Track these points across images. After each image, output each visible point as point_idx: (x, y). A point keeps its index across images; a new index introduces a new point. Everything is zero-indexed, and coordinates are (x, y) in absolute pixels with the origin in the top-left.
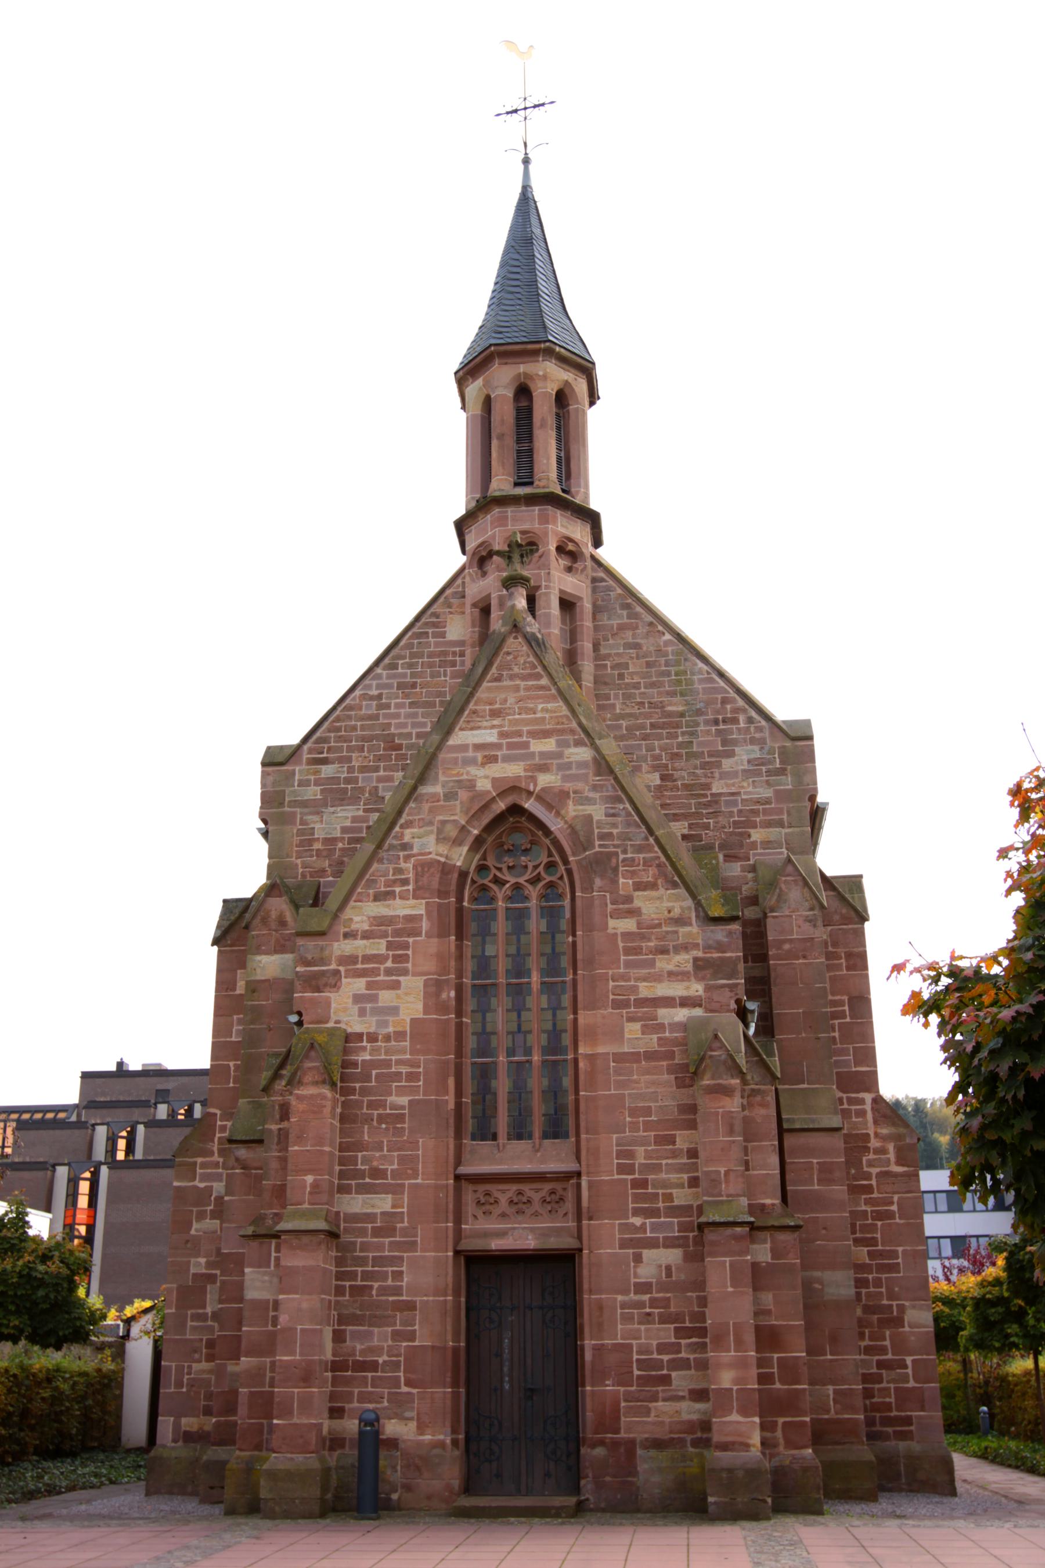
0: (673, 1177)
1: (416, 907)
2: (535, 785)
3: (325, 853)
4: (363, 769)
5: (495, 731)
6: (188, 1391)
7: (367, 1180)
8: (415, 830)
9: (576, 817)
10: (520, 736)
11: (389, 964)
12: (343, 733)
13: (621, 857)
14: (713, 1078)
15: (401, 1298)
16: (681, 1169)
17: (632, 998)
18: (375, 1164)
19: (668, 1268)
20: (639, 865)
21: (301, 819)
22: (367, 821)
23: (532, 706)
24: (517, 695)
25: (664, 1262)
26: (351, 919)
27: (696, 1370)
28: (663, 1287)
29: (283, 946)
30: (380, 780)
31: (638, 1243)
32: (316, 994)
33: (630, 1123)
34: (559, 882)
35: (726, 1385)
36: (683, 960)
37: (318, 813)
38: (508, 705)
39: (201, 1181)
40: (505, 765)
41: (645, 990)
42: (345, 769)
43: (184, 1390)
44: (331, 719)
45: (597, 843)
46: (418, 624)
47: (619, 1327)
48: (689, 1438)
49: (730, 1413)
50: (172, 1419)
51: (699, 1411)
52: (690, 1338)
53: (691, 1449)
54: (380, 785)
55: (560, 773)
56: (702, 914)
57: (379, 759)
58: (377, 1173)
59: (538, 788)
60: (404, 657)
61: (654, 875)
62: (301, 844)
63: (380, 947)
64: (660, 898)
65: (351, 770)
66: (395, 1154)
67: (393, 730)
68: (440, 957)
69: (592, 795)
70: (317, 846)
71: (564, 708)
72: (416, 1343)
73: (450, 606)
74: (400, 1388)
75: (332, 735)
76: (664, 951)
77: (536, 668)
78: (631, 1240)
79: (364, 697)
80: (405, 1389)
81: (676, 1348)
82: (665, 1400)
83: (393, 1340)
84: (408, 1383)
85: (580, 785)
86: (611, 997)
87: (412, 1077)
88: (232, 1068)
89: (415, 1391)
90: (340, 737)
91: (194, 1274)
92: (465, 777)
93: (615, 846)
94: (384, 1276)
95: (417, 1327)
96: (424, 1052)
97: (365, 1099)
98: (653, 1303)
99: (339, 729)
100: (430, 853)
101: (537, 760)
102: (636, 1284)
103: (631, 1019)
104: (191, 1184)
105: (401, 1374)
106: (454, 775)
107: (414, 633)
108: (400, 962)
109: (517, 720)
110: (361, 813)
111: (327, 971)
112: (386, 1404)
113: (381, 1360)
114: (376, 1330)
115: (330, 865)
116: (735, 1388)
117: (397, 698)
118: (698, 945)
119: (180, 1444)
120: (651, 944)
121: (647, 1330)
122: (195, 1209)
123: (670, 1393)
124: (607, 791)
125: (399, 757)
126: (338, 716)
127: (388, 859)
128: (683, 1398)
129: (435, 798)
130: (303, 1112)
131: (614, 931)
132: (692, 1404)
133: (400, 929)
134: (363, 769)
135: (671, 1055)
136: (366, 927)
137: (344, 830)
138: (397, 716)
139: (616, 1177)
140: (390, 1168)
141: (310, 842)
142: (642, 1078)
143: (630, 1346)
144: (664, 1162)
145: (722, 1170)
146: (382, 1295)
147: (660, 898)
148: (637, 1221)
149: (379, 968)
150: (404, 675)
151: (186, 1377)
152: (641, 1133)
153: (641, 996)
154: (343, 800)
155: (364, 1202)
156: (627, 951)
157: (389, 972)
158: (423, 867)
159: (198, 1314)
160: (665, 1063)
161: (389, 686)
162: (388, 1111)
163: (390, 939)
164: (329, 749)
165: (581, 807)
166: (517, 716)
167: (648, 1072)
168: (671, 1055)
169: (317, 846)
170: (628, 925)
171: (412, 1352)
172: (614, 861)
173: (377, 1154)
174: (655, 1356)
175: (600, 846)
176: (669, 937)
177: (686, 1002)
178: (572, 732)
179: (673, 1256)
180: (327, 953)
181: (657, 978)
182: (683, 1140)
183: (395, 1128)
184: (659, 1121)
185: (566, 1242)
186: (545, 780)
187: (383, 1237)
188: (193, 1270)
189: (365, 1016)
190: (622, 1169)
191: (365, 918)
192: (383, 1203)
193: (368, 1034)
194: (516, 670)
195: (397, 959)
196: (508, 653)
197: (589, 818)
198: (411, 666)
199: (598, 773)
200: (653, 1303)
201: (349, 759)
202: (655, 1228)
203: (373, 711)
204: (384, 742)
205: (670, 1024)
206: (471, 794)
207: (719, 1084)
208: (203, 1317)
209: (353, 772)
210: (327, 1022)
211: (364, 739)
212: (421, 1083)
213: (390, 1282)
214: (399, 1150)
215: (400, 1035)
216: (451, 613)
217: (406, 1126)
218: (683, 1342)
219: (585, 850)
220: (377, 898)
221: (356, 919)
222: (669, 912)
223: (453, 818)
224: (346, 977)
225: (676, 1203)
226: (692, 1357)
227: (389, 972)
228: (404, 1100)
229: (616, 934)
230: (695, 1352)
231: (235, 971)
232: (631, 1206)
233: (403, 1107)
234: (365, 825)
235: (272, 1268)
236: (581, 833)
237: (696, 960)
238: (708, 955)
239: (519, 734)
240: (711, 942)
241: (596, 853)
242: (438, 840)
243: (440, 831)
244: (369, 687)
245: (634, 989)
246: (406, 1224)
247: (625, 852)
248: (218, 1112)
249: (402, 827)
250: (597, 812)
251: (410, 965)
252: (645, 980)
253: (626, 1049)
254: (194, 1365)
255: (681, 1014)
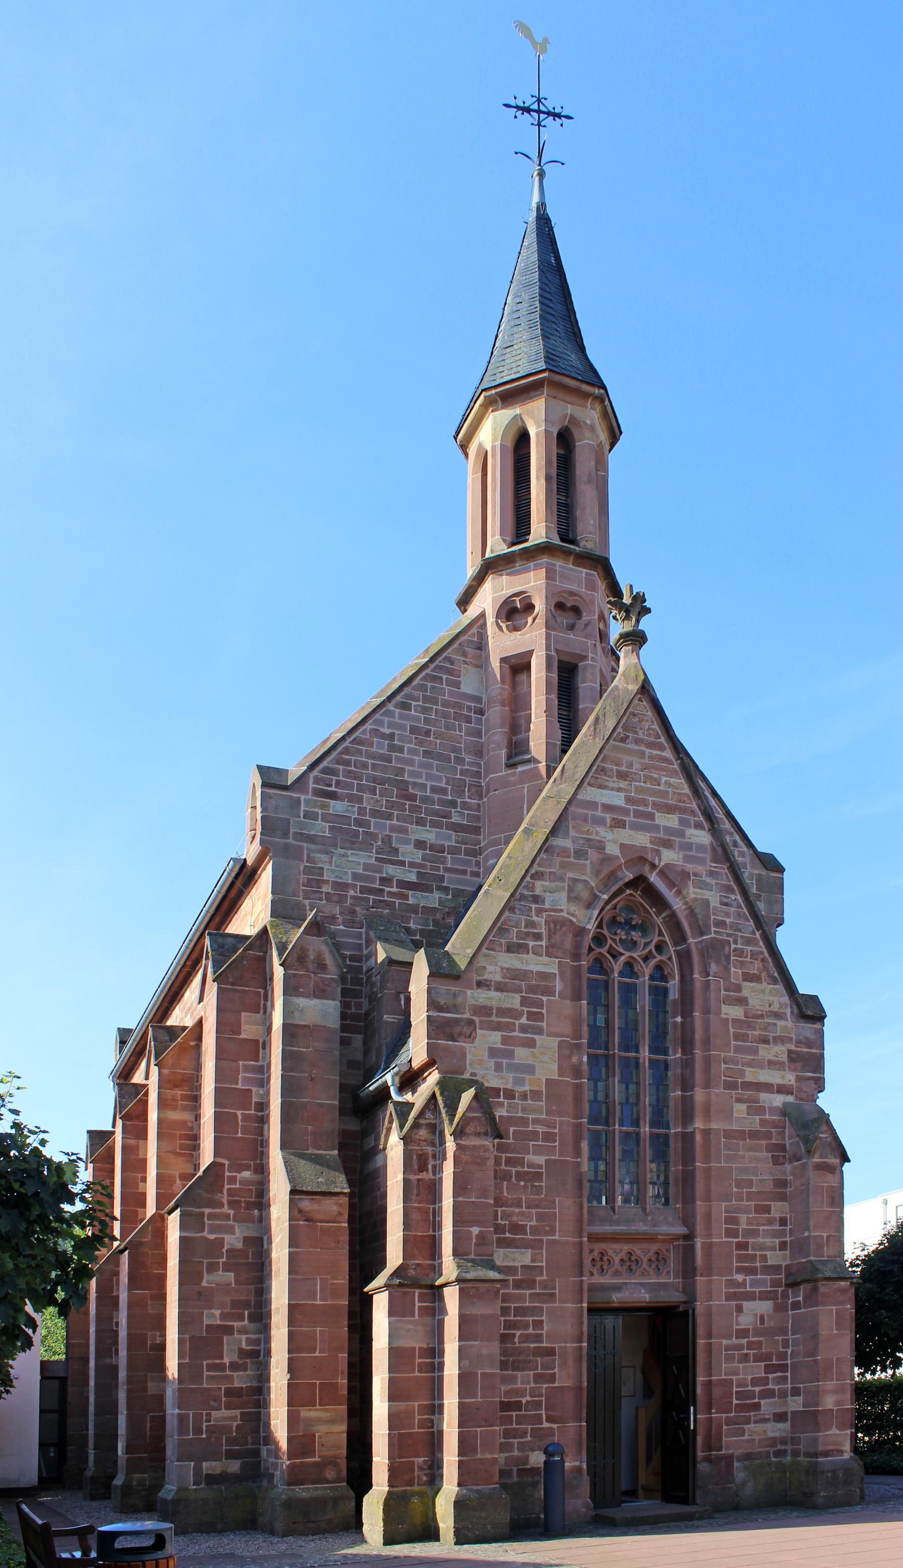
0: (768, 1241)
1: (551, 966)
2: (660, 860)
3: (335, 899)
4: (375, 813)
5: (622, 795)
6: (208, 1438)
7: (508, 1235)
8: (547, 883)
9: (695, 900)
10: (646, 805)
11: (524, 1020)
12: (353, 768)
13: (733, 946)
14: (821, 1157)
15: (541, 1345)
16: (775, 1234)
17: (740, 1080)
18: (515, 1219)
19: (762, 1317)
20: (747, 957)
21: (308, 856)
22: (380, 872)
23: (656, 776)
24: (643, 761)
25: (759, 1312)
26: (484, 968)
27: (779, 1397)
28: (757, 1333)
29: (323, 991)
30: (393, 829)
31: (739, 1296)
32: (450, 1043)
33: (736, 1192)
34: (668, 962)
35: (829, 1407)
36: (779, 1051)
37: (327, 853)
38: (634, 770)
39: (210, 1232)
40: (632, 832)
41: (751, 1075)
42: (356, 809)
43: (204, 1436)
44: (340, 749)
45: (713, 929)
46: (432, 666)
47: (724, 1365)
48: (772, 1450)
49: (831, 1429)
50: (192, 1464)
51: (779, 1430)
52: (775, 1373)
53: (774, 1459)
54: (394, 835)
55: (682, 853)
56: (796, 1011)
57: (392, 805)
58: (517, 1228)
59: (662, 863)
60: (417, 700)
61: (759, 968)
62: (309, 883)
63: (514, 1001)
64: (763, 991)
65: (362, 811)
66: (534, 1211)
67: (406, 778)
68: (576, 1022)
69: (709, 880)
70: (326, 889)
71: (686, 786)
72: (556, 1385)
73: (464, 654)
74: (542, 1424)
75: (341, 767)
76: (765, 1041)
77: (660, 738)
78: (735, 1293)
79: (375, 732)
80: (546, 1425)
81: (765, 1381)
82: (755, 1422)
83: (535, 1382)
84: (550, 1419)
85: (699, 868)
86: (723, 1078)
87: (548, 1137)
88: (240, 1118)
89: (555, 1426)
90: (350, 772)
91: (208, 1326)
92: (594, 837)
93: (728, 935)
94: (526, 1326)
95: (556, 1370)
96: (560, 1114)
97: (504, 1155)
98: (750, 1345)
99: (347, 763)
100: (562, 911)
101: (661, 835)
102: (737, 1330)
103: (739, 1100)
104: (200, 1235)
105: (543, 1412)
106: (583, 833)
107: (427, 674)
108: (534, 1020)
109: (642, 787)
110: (373, 861)
111: (461, 1019)
112: (529, 1438)
113: (524, 1401)
114: (519, 1374)
115: (341, 913)
116: (835, 1409)
117: (410, 742)
118: (791, 1039)
119: (203, 1486)
120: (757, 1033)
121: (744, 1367)
122: (205, 1261)
123: (759, 1417)
124: (722, 879)
125: (415, 809)
126: (347, 748)
127: (519, 910)
128: (769, 1420)
129: (564, 852)
130: (467, 1163)
131: (725, 1016)
132: (776, 1424)
133: (534, 985)
134: (375, 813)
135: (769, 1135)
136: (498, 978)
137: (356, 876)
138: (411, 763)
139: (724, 1239)
140: (529, 1224)
141: (320, 883)
142: (746, 1154)
143: (732, 1380)
144: (761, 1228)
145: (825, 1235)
146: (524, 1342)
147: (763, 991)
148: (740, 1278)
149: (514, 1024)
150: (418, 719)
151: (205, 1424)
152: (745, 1203)
153: (746, 1080)
154: (354, 843)
155: (505, 1256)
156: (737, 1037)
157: (523, 1029)
158: (557, 924)
159: (215, 1364)
160: (764, 1142)
161: (402, 727)
162: (526, 1169)
163: (524, 994)
164: (338, 783)
165: (699, 891)
166: (642, 784)
167: (750, 1149)
168: (769, 1135)
169: (326, 889)
170: (734, 1012)
171: (553, 1393)
172: (727, 949)
173: (517, 1210)
174: (750, 1388)
175: (716, 932)
176: (770, 1028)
177: (782, 1089)
178: (693, 812)
179: (765, 1307)
180: (460, 999)
181: (758, 1065)
182: (778, 1209)
183: (533, 1186)
184: (759, 1193)
185: (674, 1297)
186: (669, 856)
187: (524, 1289)
188: (206, 1322)
189: (502, 1071)
190: (732, 1233)
191: (498, 969)
192: (524, 1258)
193: (505, 1090)
194: (641, 735)
195: (531, 1016)
196: (634, 715)
197: (706, 903)
198: (425, 710)
199: (714, 860)
200: (750, 1345)
201: (360, 800)
202: (754, 1283)
203: (384, 751)
204: (398, 788)
205: (770, 1108)
206: (600, 856)
207: (825, 1162)
208: (221, 1367)
209: (365, 815)
210: (462, 1074)
211: (375, 780)
212: (557, 1144)
213: (531, 1331)
214: (537, 1207)
215: (536, 1094)
216: (465, 662)
217: (543, 1184)
218: (770, 1376)
219: (702, 934)
220: (510, 948)
221: (490, 968)
222: (770, 1006)
223: (583, 878)
224: (480, 1029)
225: (770, 1263)
226: (776, 1388)
227: (523, 1029)
228: (541, 1160)
229: (728, 1019)
230: (778, 1384)
231: (239, 1012)
232: (735, 1265)
233: (540, 1167)
234: (378, 875)
235: (417, 1317)
236: (700, 917)
237: (790, 1052)
238: (799, 1049)
239: (644, 803)
240: (801, 1038)
241: (712, 939)
242: (569, 899)
243: (571, 890)
244: (381, 723)
245: (742, 1073)
246: (545, 1277)
247: (736, 942)
248: (227, 1163)
249: (532, 877)
250: (714, 898)
251: (544, 1024)
252: (750, 1066)
253: (734, 1127)
254: (213, 1413)
255: (779, 1100)
